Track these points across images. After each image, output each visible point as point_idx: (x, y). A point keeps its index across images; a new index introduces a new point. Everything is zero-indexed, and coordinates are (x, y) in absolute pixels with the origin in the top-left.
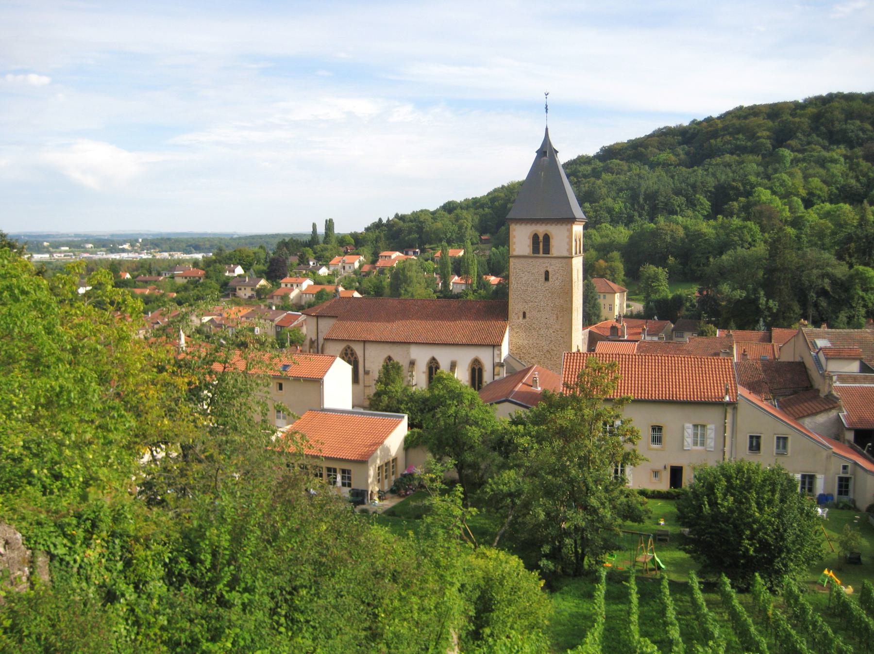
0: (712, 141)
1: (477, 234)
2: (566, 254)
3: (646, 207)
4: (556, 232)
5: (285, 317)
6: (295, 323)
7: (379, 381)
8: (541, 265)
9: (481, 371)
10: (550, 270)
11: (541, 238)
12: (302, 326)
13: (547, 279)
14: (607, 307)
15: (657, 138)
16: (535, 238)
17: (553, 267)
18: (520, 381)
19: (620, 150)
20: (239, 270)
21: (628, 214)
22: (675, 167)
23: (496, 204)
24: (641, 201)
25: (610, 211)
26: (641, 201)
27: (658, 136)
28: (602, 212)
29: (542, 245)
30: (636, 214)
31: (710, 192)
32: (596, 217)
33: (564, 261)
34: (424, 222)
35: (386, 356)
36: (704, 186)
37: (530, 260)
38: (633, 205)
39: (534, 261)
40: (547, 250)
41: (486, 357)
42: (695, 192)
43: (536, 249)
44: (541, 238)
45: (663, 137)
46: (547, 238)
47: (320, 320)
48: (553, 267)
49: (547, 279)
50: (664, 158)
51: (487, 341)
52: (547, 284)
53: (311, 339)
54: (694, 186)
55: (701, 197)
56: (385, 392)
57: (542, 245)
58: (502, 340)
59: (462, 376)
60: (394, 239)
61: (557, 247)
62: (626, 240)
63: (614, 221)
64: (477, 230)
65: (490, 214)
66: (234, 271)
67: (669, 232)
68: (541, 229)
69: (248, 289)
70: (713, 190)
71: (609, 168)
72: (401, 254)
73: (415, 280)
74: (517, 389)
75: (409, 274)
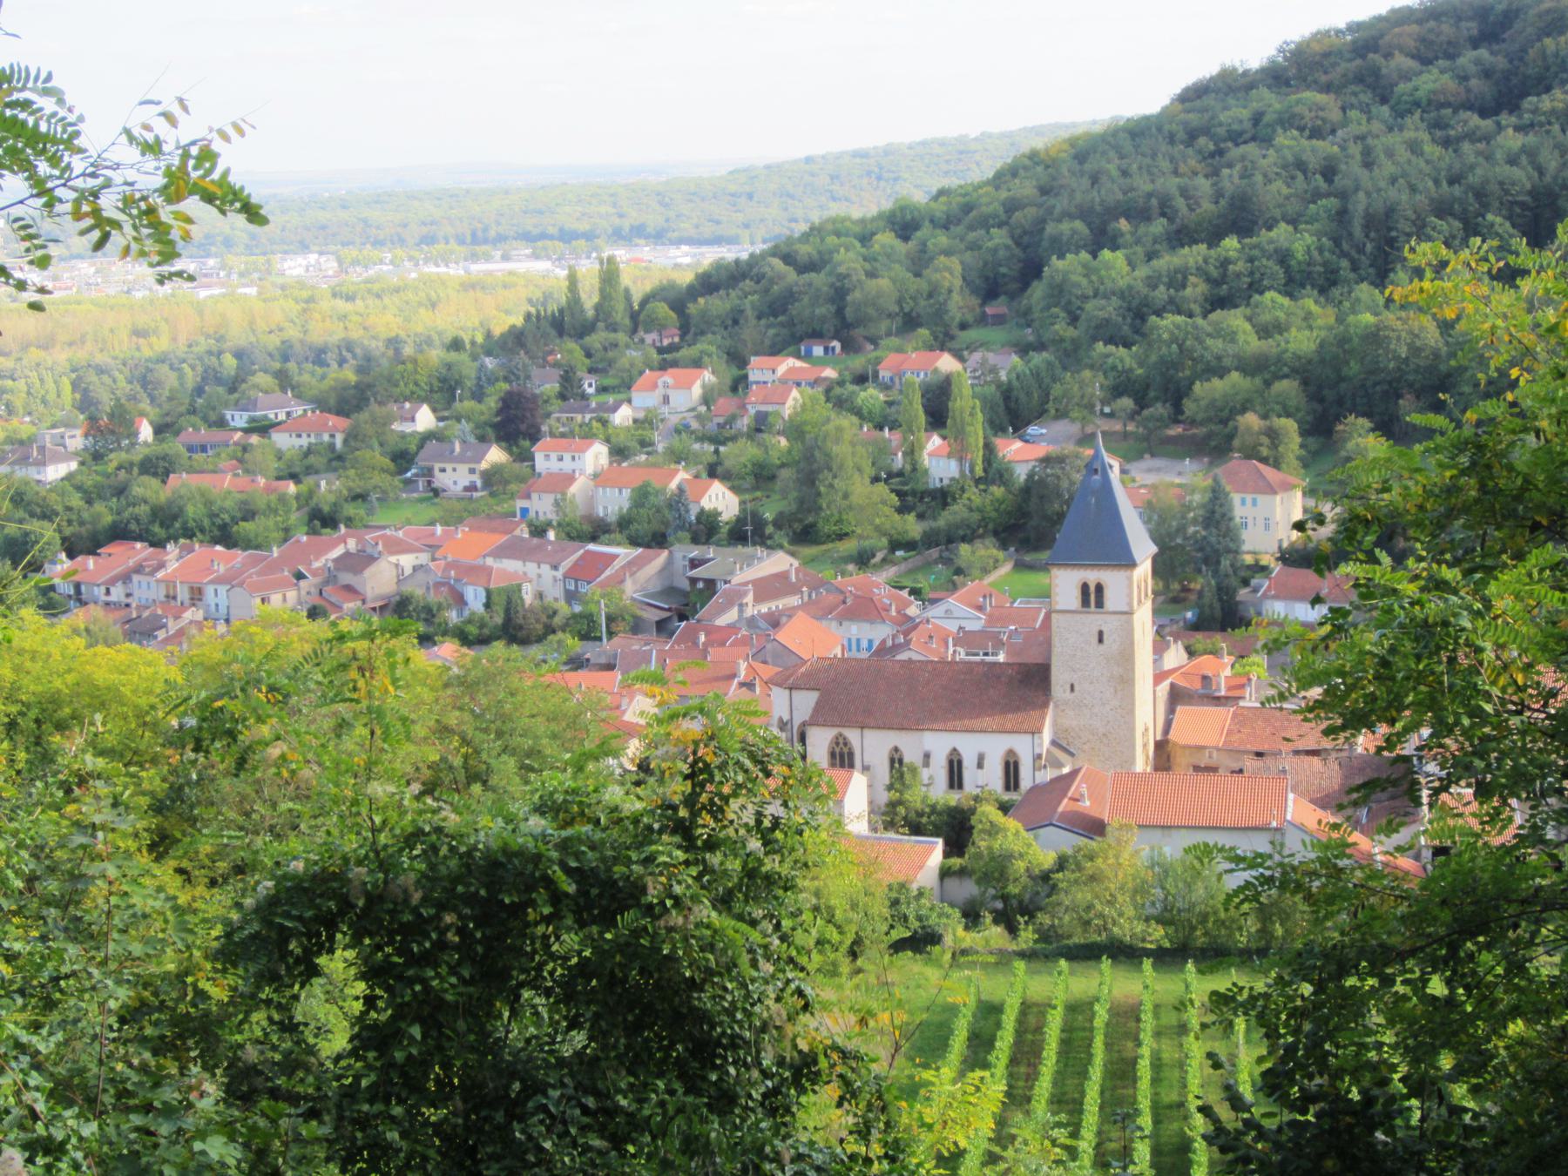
0: (1548, 41)
1: (975, 301)
2: (1125, 609)
3: (1369, 247)
4: (1111, 579)
5: (582, 558)
6: (608, 573)
7: (890, 788)
8: (1094, 621)
9: (1016, 765)
10: (1105, 630)
11: (1092, 588)
12: (622, 581)
13: (1101, 640)
14: (1260, 522)
15: (1415, 28)
16: (1085, 588)
17: (1109, 624)
18: (1065, 795)
19: (1326, 55)
20: (425, 419)
21: (1325, 264)
22: (1455, 112)
23: (1018, 215)
24: (1358, 231)
25: (1283, 257)
26: (1358, 231)
27: (1420, 22)
28: (1264, 261)
29: (1092, 597)
30: (1345, 263)
31: (1522, 205)
32: (1252, 273)
33: (1124, 617)
34: (848, 276)
35: (891, 746)
36: (1507, 192)
37: (1078, 617)
38: (1336, 241)
39: (1083, 616)
40: (1100, 604)
41: (1023, 746)
42: (1486, 207)
43: (1085, 602)
44: (1092, 588)
45: (1432, 24)
46: (1099, 589)
47: (794, 693)
48: (1109, 624)
49: (1101, 640)
50: (1430, 86)
51: (1025, 727)
52: (1101, 647)
53: (781, 719)
54: (1480, 194)
55: (1498, 220)
56: (900, 802)
57: (1092, 597)
58: (1043, 725)
59: (993, 777)
60: (776, 316)
61: (1112, 600)
62: (1313, 347)
63: (1293, 285)
64: (975, 291)
65: (1007, 247)
66: (413, 419)
67: (1404, 334)
68: (1092, 576)
69: (463, 469)
70: (1526, 198)
71: (1293, 116)
72: (799, 364)
73: (850, 463)
74: (1060, 809)
75: (836, 449)
